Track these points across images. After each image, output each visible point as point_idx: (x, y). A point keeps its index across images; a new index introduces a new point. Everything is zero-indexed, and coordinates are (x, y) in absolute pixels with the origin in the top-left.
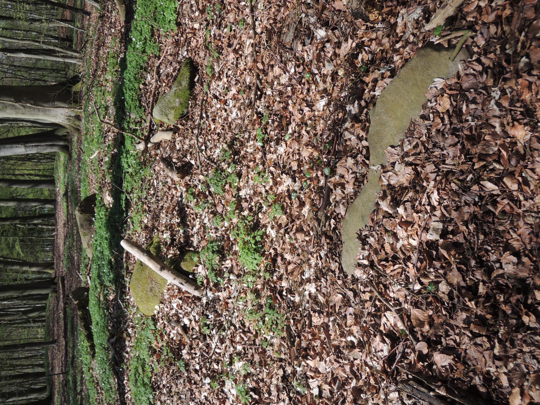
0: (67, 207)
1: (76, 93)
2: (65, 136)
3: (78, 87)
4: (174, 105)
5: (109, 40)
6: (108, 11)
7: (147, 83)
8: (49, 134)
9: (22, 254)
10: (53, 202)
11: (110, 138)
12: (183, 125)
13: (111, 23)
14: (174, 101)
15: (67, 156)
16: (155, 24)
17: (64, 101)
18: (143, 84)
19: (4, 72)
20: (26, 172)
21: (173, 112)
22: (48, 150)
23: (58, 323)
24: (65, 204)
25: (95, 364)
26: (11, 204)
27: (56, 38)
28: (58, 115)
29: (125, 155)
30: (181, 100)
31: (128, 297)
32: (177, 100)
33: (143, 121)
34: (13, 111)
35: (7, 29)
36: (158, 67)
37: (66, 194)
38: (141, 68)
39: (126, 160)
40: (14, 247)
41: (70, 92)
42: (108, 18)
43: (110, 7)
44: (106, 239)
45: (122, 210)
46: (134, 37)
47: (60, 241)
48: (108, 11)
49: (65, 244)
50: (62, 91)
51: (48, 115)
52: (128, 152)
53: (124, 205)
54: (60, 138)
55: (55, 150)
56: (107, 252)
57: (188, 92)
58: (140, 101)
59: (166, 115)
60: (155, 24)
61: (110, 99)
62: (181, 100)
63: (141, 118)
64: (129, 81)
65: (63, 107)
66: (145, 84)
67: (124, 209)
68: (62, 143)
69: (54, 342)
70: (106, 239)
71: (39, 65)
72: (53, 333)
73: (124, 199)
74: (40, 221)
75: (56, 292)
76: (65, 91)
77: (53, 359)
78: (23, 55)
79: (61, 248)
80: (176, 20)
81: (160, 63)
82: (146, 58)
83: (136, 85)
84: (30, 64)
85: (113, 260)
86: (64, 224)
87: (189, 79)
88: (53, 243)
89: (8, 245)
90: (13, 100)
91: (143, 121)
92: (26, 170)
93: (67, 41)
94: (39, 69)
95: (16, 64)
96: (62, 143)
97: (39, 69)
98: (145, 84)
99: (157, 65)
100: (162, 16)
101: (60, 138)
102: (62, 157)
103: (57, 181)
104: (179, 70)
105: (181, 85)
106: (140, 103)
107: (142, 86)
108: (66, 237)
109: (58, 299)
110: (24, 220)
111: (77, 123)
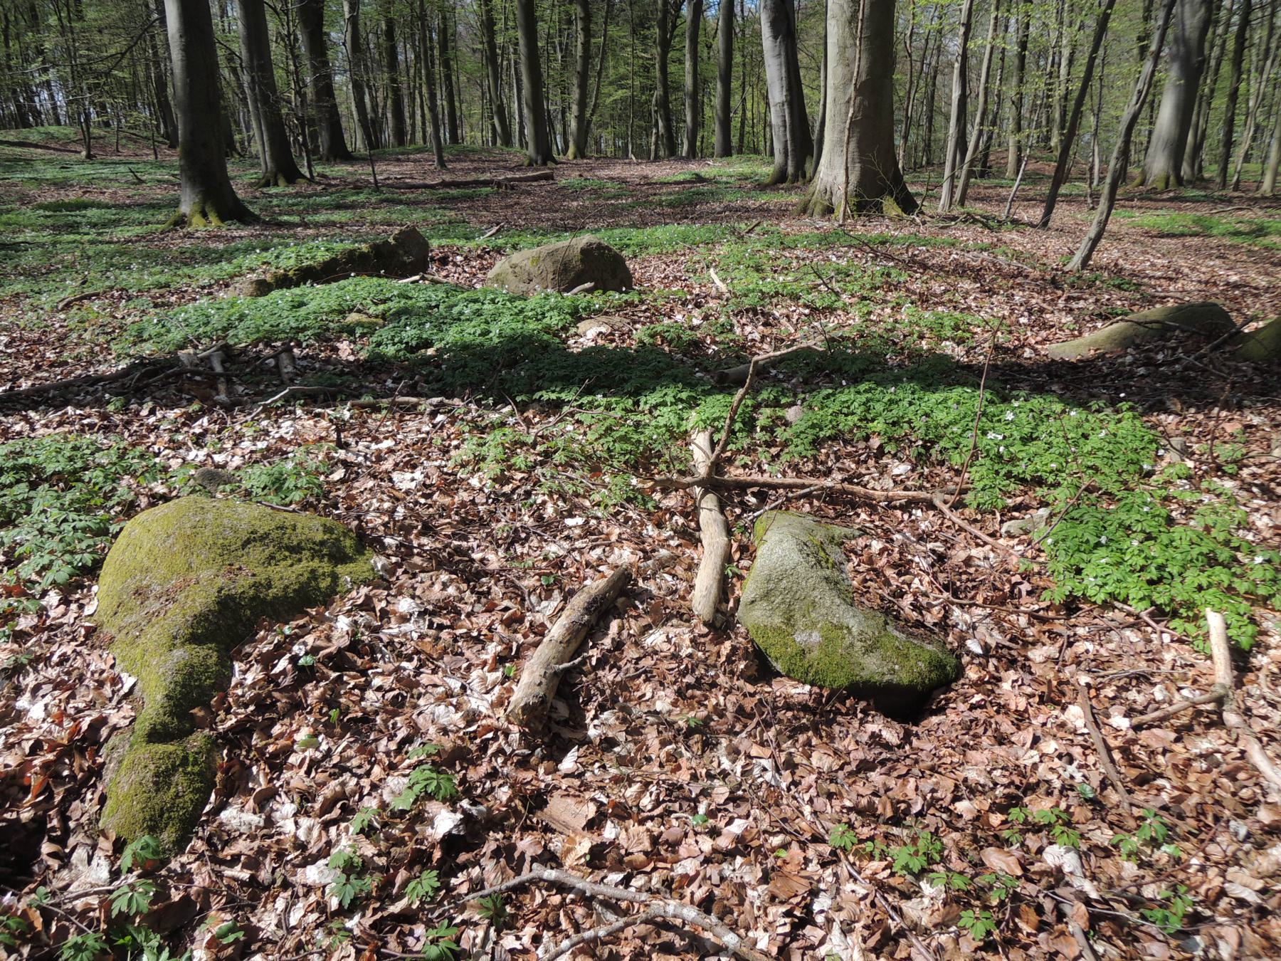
0: (677, 183)
1: (879, 208)
2: (804, 176)
3: (891, 207)
4: (800, 624)
5: (997, 308)
6: (1068, 299)
7: (885, 460)
8: (805, 143)
9: (608, 101)
10: (693, 155)
11: (748, 329)
12: (729, 660)
13: (1042, 311)
14: (814, 624)
15: (767, 180)
16: (1061, 497)
17: (861, 183)
18: (881, 447)
19: (924, 57)
20: (749, 106)
21: (777, 621)
22: (778, 147)
23: (476, 169)
24: (681, 178)
25: (237, 297)
26: (688, 81)
27: (987, 148)
28: (834, 170)
29: (684, 395)
30: (816, 654)
31: (299, 412)
32: (816, 637)
33: (774, 451)
34: (839, 81)
35: (1002, 59)
36: (931, 506)
37: (699, 179)
38: (928, 445)
39: (669, 399)
40: (622, 87)
41: (880, 194)
42: (1053, 302)
43: (1082, 304)
44: (485, 333)
45: (533, 392)
46: (1017, 412)
47: (617, 171)
48: (1068, 299)
49: (612, 179)
50: (882, 180)
51: (832, 150)
52: (692, 403)
53: (546, 396)
54: (800, 167)
55: (778, 158)
56: (452, 335)
57: (842, 681)
58: (833, 438)
59: (766, 595)
60: (1061, 497)
61: (849, 321)
62: (816, 654)
63: (785, 444)
64: (891, 402)
65: (847, 183)
66: (881, 452)
67: (537, 396)
68: (790, 170)
69: (442, 163)
70: (485, 333)
71: (938, 119)
72: (459, 160)
73: (563, 396)
74: (661, 130)
75: (530, 164)
76: (880, 184)
77: (415, 161)
78: (956, 94)
79: (603, 173)
80: (1085, 598)
81: (941, 512)
82: (956, 460)
83: (878, 425)
84: (940, 104)
85: (430, 352)
86: (646, 177)
87: (889, 683)
88: (621, 154)
89: (623, 77)
90: (863, 78)
91: (774, 451)
92: (745, 103)
93: (984, 167)
94: (930, 119)
95: (939, 77)
96: (790, 170)
97: (930, 119)
98: (881, 452)
99: (938, 502)
100: (1093, 540)
101: (800, 167)
102: (766, 171)
103: (725, 160)
104: (920, 624)
105: (868, 651)
106: (829, 438)
107: (875, 442)
108: (623, 181)
109: (519, 167)
110: (664, 103)
111: (818, 209)
